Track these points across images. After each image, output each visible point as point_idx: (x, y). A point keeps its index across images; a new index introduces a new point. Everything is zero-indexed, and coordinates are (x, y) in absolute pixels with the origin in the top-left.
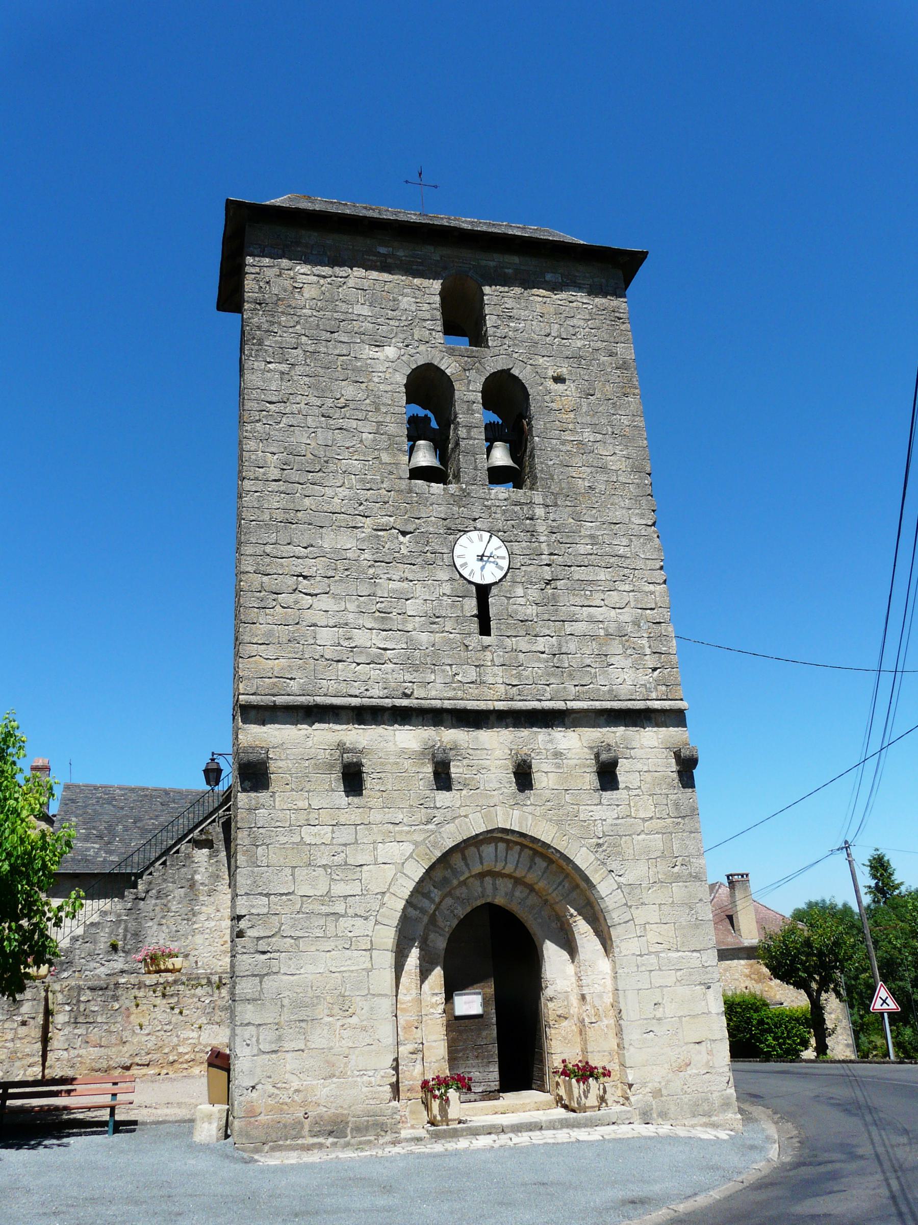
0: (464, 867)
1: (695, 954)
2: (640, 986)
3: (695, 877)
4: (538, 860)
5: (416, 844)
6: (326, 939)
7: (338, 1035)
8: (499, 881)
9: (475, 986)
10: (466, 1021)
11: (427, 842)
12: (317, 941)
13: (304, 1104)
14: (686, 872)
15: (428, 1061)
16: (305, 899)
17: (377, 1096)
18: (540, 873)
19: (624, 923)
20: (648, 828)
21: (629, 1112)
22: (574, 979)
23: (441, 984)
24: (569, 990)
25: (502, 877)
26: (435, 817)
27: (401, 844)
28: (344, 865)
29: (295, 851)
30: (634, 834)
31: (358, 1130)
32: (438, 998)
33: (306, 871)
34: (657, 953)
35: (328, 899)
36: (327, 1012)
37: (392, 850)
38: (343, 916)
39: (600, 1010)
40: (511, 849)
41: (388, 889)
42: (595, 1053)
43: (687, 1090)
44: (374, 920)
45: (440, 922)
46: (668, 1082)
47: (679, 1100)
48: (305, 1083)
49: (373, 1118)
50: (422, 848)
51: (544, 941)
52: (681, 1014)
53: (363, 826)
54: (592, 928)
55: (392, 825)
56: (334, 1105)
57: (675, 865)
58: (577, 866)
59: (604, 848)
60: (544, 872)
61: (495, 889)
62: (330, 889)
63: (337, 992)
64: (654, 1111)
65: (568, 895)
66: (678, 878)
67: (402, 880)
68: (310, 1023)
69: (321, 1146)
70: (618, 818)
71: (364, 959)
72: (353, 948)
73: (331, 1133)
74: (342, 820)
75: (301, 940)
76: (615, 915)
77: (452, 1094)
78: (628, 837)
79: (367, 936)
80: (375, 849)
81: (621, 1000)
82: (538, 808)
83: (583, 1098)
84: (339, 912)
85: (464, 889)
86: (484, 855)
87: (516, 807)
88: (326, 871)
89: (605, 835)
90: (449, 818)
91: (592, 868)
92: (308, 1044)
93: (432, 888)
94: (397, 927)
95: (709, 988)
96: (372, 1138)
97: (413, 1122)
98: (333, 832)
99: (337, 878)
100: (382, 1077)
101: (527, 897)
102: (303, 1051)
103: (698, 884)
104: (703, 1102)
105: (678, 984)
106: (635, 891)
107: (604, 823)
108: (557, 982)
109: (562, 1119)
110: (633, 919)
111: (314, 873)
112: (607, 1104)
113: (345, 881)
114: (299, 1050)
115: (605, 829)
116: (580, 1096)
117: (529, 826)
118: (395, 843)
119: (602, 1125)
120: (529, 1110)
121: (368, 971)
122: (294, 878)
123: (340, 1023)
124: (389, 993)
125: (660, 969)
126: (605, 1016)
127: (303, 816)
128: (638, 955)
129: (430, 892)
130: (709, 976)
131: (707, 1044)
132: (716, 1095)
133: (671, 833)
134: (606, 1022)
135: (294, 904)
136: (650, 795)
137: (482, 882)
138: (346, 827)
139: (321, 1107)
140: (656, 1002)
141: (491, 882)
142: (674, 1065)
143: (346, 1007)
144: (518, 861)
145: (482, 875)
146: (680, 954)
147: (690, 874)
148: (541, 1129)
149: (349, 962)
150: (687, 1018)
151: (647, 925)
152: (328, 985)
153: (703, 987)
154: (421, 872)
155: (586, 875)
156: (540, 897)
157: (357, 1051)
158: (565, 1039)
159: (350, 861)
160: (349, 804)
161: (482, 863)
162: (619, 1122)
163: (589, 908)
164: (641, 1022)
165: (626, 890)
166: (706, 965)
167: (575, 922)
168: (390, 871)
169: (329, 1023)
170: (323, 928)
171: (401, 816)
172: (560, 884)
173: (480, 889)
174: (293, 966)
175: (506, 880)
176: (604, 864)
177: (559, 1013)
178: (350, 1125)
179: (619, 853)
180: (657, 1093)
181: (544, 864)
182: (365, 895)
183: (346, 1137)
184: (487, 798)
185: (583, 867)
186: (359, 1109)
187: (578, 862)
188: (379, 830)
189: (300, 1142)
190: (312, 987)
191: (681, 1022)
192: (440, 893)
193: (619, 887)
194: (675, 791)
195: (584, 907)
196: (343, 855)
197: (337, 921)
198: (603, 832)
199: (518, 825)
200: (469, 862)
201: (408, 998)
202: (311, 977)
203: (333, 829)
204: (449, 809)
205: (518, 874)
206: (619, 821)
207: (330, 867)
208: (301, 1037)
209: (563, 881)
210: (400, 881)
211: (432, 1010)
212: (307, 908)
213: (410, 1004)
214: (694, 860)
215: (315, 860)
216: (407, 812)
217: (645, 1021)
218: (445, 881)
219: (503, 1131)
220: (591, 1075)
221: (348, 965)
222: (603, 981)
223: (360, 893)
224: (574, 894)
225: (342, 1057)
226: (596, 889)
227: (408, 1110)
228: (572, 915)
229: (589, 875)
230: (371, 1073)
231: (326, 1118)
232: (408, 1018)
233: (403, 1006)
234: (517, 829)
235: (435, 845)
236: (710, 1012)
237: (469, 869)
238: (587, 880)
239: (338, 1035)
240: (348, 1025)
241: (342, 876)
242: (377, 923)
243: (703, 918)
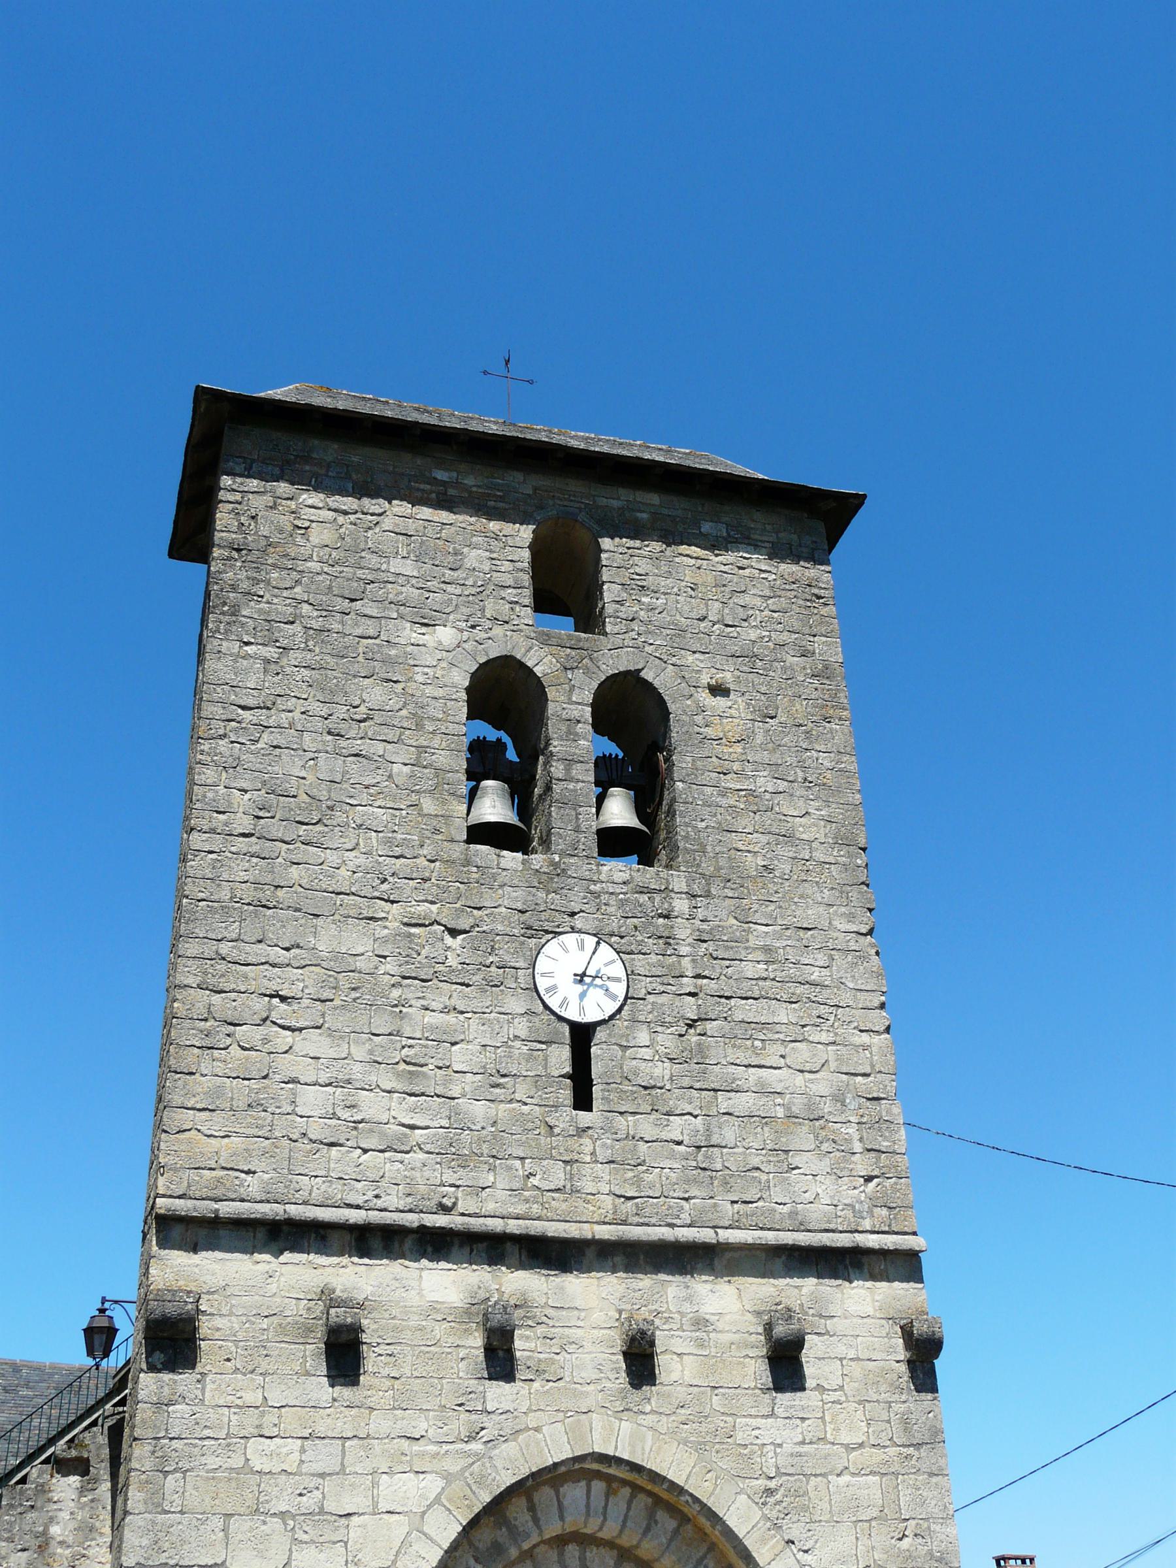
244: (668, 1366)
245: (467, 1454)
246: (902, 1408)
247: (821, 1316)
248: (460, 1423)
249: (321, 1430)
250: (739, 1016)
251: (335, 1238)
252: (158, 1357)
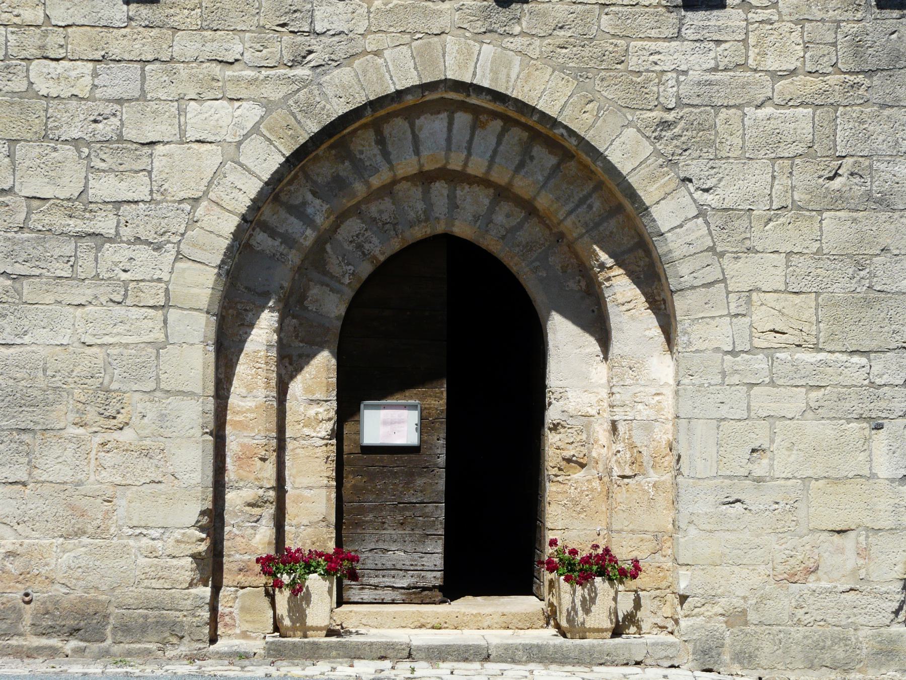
0: (379, 158)
1: (856, 359)
2: (724, 412)
3: (879, 202)
4: (538, 151)
5: (268, 106)
6: (75, 282)
7: (93, 461)
8: (463, 192)
9: (407, 393)
10: (385, 456)
11: (291, 102)
12: (57, 284)
13: (24, 576)
14: (858, 191)
15: (294, 522)
16: (36, 203)
17: (166, 574)
18: (540, 178)
19: (704, 286)
20: (781, 93)
21: (672, 645)
22: (604, 393)
23: (328, 384)
24: (593, 412)
25: (470, 184)
26: (310, 52)
27: (237, 104)
28: (117, 141)
29: (17, 109)
30: (748, 104)
31: (125, 629)
32: (321, 410)
33: (38, 150)
34: (769, 352)
35: (81, 206)
36: (72, 417)
37: (216, 116)
38: (110, 240)
39: (644, 453)
40: (483, 126)
41: (206, 193)
42: (624, 534)
43: (803, 618)
44: (174, 252)
45: (334, 265)
46: (763, 599)
47: (782, 635)
48: (27, 541)
49: (157, 613)
50: (279, 115)
51: (549, 314)
52: (810, 473)
53: (157, 65)
54: (644, 294)
55: (219, 66)
56: (81, 583)
57: (836, 175)
58: (615, 168)
59: (677, 131)
60: (548, 179)
61: (453, 205)
62: (86, 186)
63: (96, 382)
64: (726, 649)
65: (597, 225)
66: (837, 202)
67: (235, 177)
68: (39, 435)
69: (53, 652)
70: (715, 69)
71: (150, 324)
72: (129, 302)
73: (74, 632)
74: (115, 51)
75: (25, 282)
76: (684, 269)
77: (317, 584)
78: (733, 110)
79: (159, 280)
80: (181, 112)
81: (682, 437)
82: (537, 42)
83: (580, 612)
84: (103, 232)
85: (387, 204)
86: (422, 135)
87: (487, 38)
88: (79, 152)
89: (680, 104)
90: (340, 55)
91: (644, 171)
92: (36, 472)
93: (309, 197)
94: (220, 267)
95: (879, 427)
96: (153, 646)
97: (245, 627)
98: (95, 74)
99: (103, 165)
100: (178, 541)
101: (520, 226)
102: (24, 484)
103: (883, 216)
104: (834, 643)
105: (809, 414)
106: (736, 224)
107: (682, 78)
108: (569, 394)
109: (532, 646)
110: (724, 280)
111: (54, 154)
112: (639, 628)
113: (120, 174)
114: (16, 483)
115: (684, 90)
116: (574, 608)
117: (513, 76)
118: (225, 103)
119: (614, 663)
120: (489, 627)
121: (159, 347)
122: (13, 162)
123: (98, 439)
124: (198, 390)
125: (772, 383)
126: (652, 467)
127: (32, 39)
128: (728, 352)
129: (304, 204)
130: (883, 404)
131: (859, 535)
132: (864, 632)
133: (835, 106)
134: (654, 477)
135: (13, 212)
136: (797, 22)
137: (426, 193)
138: (122, 64)
139: (57, 586)
140: (755, 445)
141: (445, 192)
142: (780, 568)
143: (112, 411)
144: (495, 152)
145: (425, 178)
146: (822, 356)
147: (869, 196)
148: (487, 658)
149: (120, 328)
150: (821, 482)
151: (754, 296)
152: (77, 370)
153: (865, 425)
154: (275, 161)
155: (630, 186)
156: (548, 227)
157: (129, 493)
158: (577, 504)
159: (130, 133)
160: (130, 19)
161: (417, 152)
162: (648, 661)
163: (640, 253)
164: (718, 481)
165: (716, 220)
166: (878, 381)
167: (608, 279)
168: (211, 157)
169: (77, 437)
170: (72, 261)
171: (240, 48)
172: (582, 201)
173: (420, 206)
174: (8, 330)
175: (476, 188)
176: (671, 163)
177: (567, 454)
178: (112, 620)
179: (710, 144)
180: (735, 618)
181: (552, 160)
182: (158, 203)
183: (104, 641)
184: (425, 16)
185: (624, 167)
186: (130, 594)
187: (615, 157)
188: (191, 76)
189: (14, 642)
190: (45, 370)
191: (806, 489)
192: (326, 207)
193: (701, 214)
194: (859, 15)
195: (631, 250)
196: (115, 121)
197: (99, 248)
198: (679, 98)
199: (489, 76)
200: (390, 149)
201: (250, 403)
202: (43, 352)
203: (95, 70)
204: (343, 37)
205: (500, 176)
206: (719, 76)
207: (88, 144)
208: (21, 460)
209: (589, 195)
210: (231, 178)
211: (306, 431)
212: (39, 220)
213: (252, 416)
214: (883, 167)
215: (57, 128)
216: (252, 40)
217: (727, 482)
218: (339, 184)
219: (410, 656)
220: (601, 573)
221: (118, 334)
222: (657, 398)
223: (148, 198)
224: (612, 224)
225: (99, 500)
226: (649, 214)
227: (237, 604)
228: (602, 266)
229: (635, 186)
230: (155, 533)
231: (66, 604)
232: (246, 440)
233: (237, 418)
234: (486, 84)
235: (308, 109)
236: (873, 476)
237: (389, 162)
238: (632, 194)
239: (93, 461)
240: (114, 444)
241: (111, 162)
242: (180, 256)
243: (884, 288)
245: (292, 80)
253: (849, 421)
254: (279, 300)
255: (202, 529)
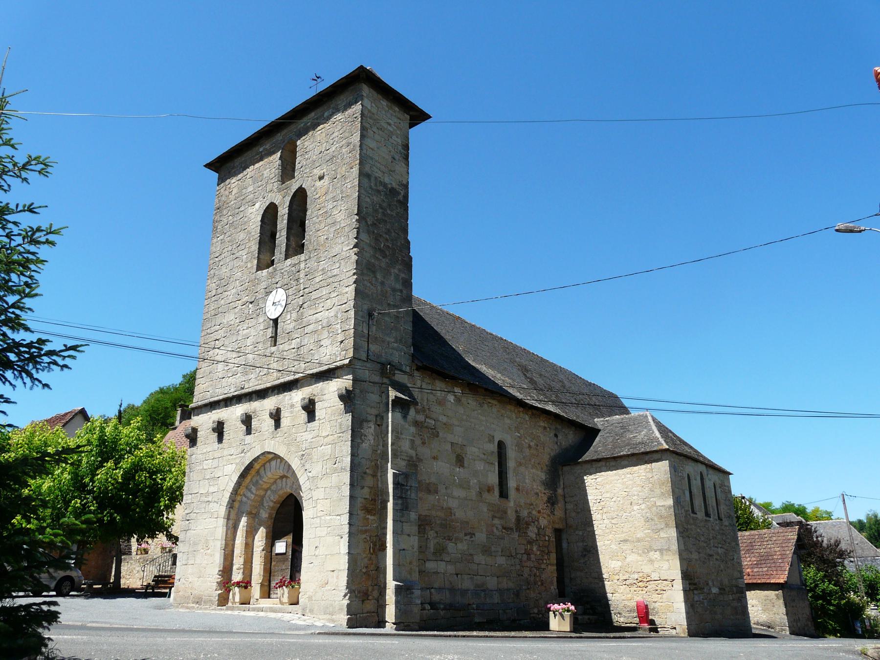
95: (342, 538)
133: (336, 443)
146: (331, 517)
230: (211, 576)
236: (340, 553)
244: (284, 422)
245: (240, 457)
246: (339, 421)
247: (322, 395)
248: (240, 450)
249: (216, 456)
250: (313, 298)
251: (338, 372)
252: (273, 472)
253: (336, 536)
254: (247, 514)
255: (219, 575)
